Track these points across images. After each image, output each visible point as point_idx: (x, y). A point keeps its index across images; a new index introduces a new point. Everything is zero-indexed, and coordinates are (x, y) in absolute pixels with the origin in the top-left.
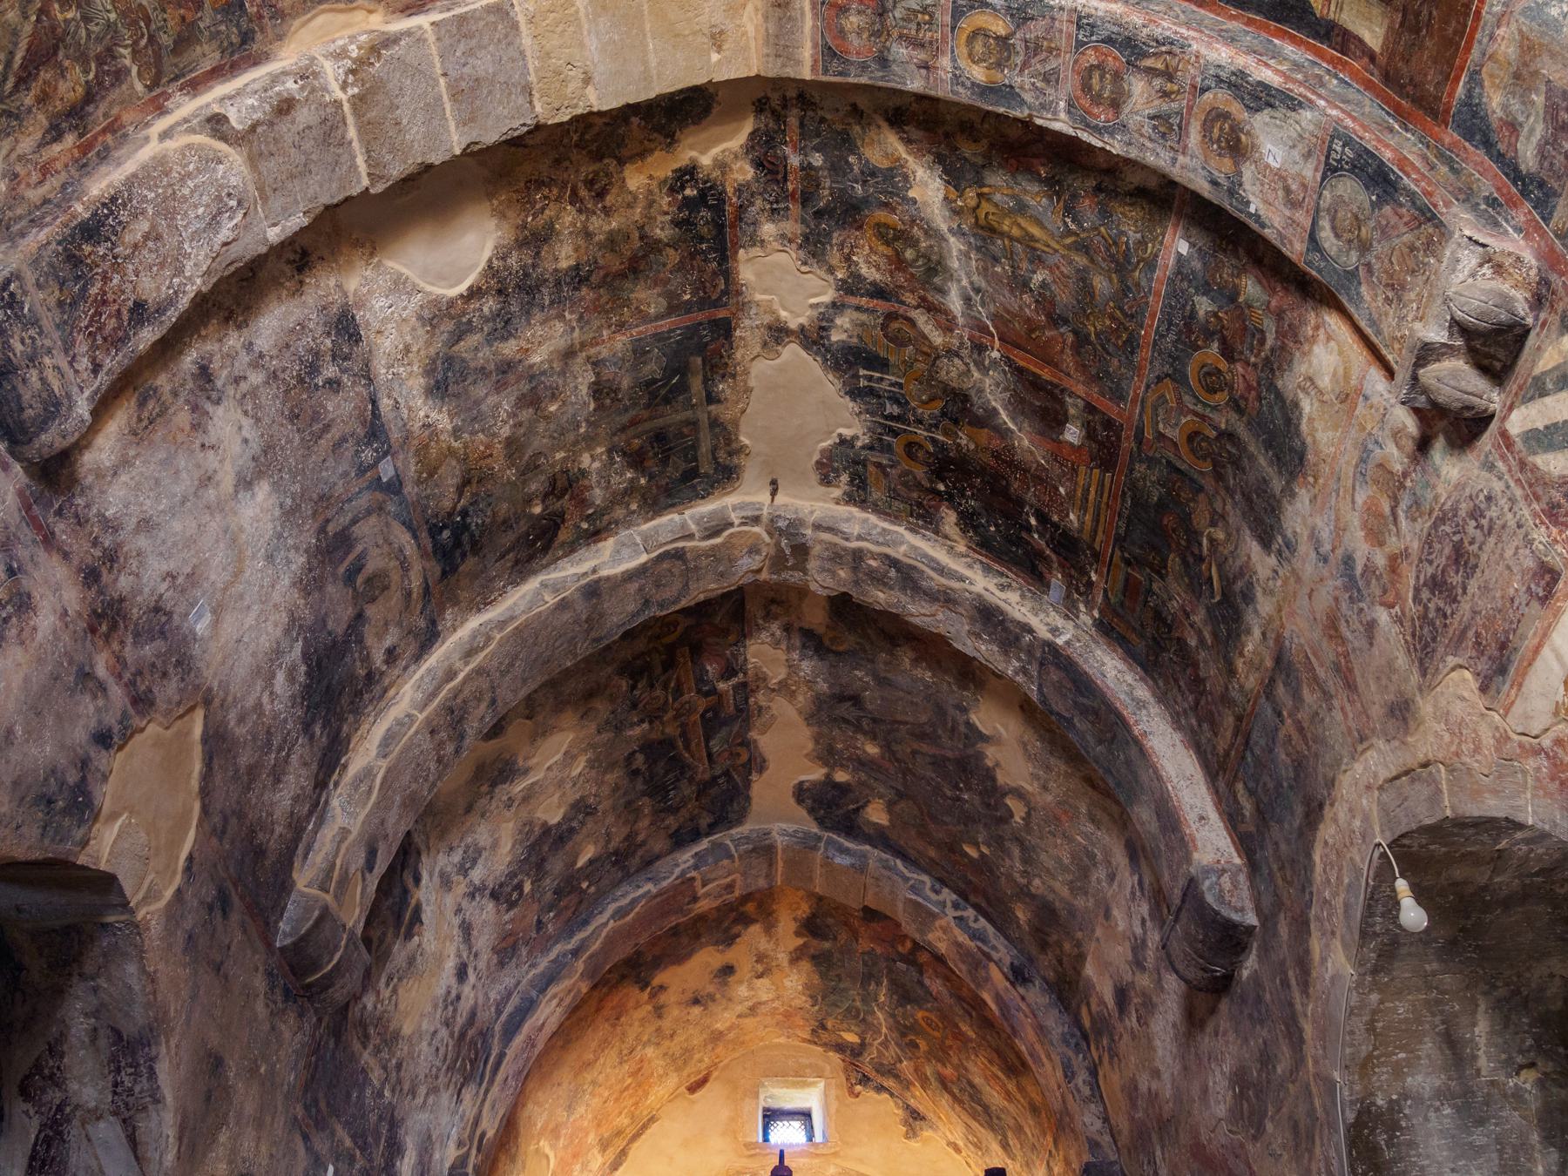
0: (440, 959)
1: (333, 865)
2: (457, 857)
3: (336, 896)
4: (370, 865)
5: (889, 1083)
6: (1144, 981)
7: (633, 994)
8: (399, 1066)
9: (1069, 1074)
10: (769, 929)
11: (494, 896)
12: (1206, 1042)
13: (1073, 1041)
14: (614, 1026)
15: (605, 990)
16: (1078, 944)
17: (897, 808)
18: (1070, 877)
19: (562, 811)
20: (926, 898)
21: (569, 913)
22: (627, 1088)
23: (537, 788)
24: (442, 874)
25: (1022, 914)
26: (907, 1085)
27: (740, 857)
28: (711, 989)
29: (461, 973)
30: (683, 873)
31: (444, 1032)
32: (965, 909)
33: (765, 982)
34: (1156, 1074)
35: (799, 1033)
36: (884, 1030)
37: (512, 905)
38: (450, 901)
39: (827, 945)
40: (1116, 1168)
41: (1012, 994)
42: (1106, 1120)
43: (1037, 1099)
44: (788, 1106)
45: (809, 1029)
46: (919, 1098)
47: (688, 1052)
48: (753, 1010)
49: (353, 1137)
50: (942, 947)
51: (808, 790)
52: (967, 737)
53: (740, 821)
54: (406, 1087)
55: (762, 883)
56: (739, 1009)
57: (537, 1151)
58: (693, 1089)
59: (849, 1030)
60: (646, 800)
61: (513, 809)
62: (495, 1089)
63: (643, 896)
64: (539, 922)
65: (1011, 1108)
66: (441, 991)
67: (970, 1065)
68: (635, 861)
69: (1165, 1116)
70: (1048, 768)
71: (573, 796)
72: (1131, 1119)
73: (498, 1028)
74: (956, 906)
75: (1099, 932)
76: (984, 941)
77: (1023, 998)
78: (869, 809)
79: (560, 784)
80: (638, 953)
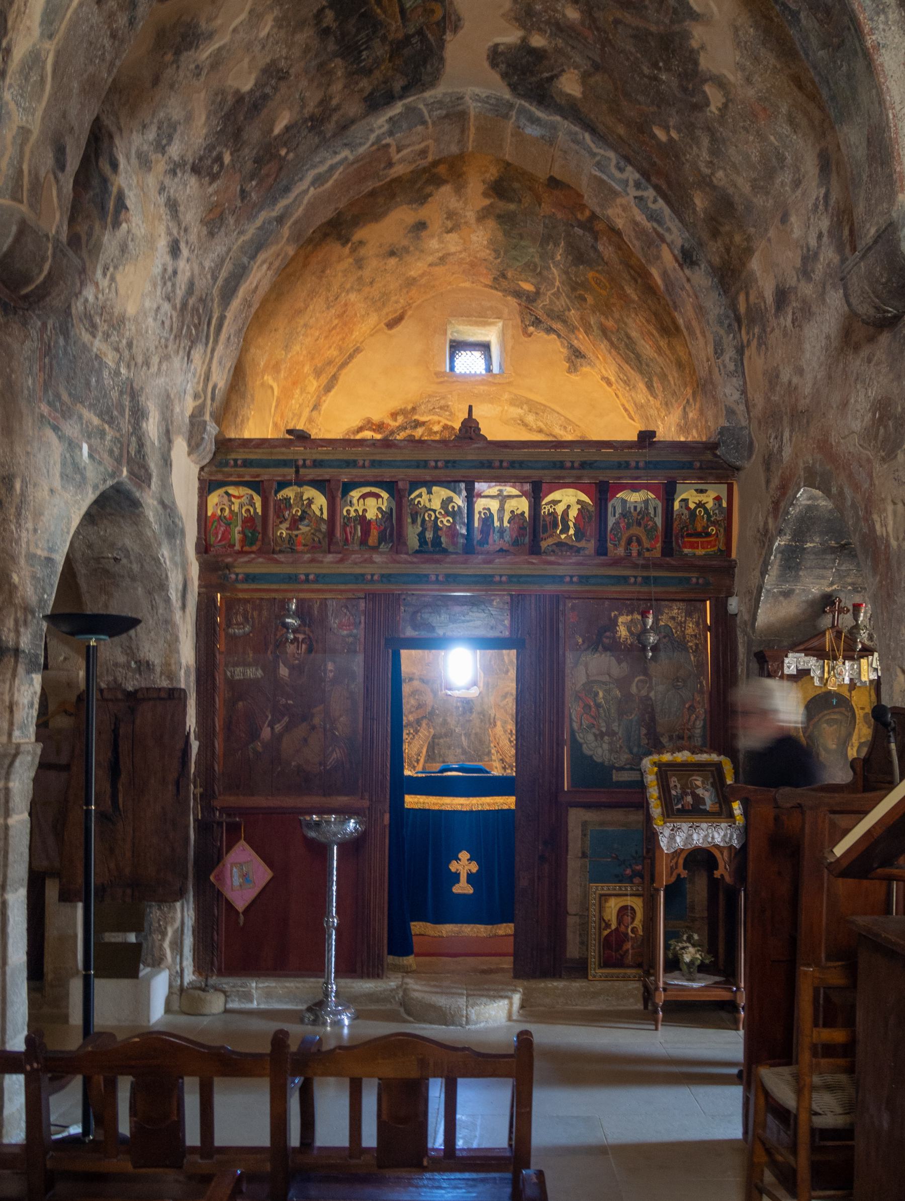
0: (151, 241)
1: (20, 172)
2: (151, 135)
3: (31, 206)
4: (60, 165)
5: (557, 326)
6: (807, 290)
7: (335, 249)
8: (130, 345)
9: (719, 351)
10: (459, 189)
11: (195, 170)
12: (856, 364)
13: (727, 322)
14: (320, 278)
15: (310, 248)
16: (749, 239)
17: (592, 81)
18: (754, 175)
19: (253, 77)
20: (611, 176)
21: (271, 180)
22: (334, 328)
23: (224, 53)
24: (140, 155)
25: (700, 201)
26: (573, 329)
27: (434, 123)
28: (405, 242)
29: (174, 250)
30: (379, 139)
31: (166, 307)
32: (646, 189)
33: (453, 236)
34: (800, 371)
35: (482, 280)
36: (557, 283)
37: (214, 178)
38: (151, 181)
39: (512, 207)
40: (746, 432)
41: (679, 275)
42: (744, 392)
43: (684, 358)
44: (472, 339)
45: (491, 277)
46: (582, 341)
47: (385, 297)
48: (443, 260)
49: (100, 416)
50: (620, 223)
51: (502, 53)
52: (675, 11)
53: (432, 84)
54: (140, 360)
55: (454, 149)
56: (430, 259)
57: (263, 385)
58: (391, 325)
59: (526, 281)
60: (339, 61)
61: (202, 78)
62: (220, 347)
63: (340, 163)
64: (243, 191)
65: (660, 360)
66: (157, 270)
67: (629, 321)
68: (330, 127)
69: (800, 409)
70: (756, 60)
71: (263, 60)
72: (768, 399)
73: (215, 292)
74: (638, 186)
75: (771, 233)
76: (659, 222)
77: (688, 280)
78: (563, 79)
79: (248, 48)
80: (339, 214)
